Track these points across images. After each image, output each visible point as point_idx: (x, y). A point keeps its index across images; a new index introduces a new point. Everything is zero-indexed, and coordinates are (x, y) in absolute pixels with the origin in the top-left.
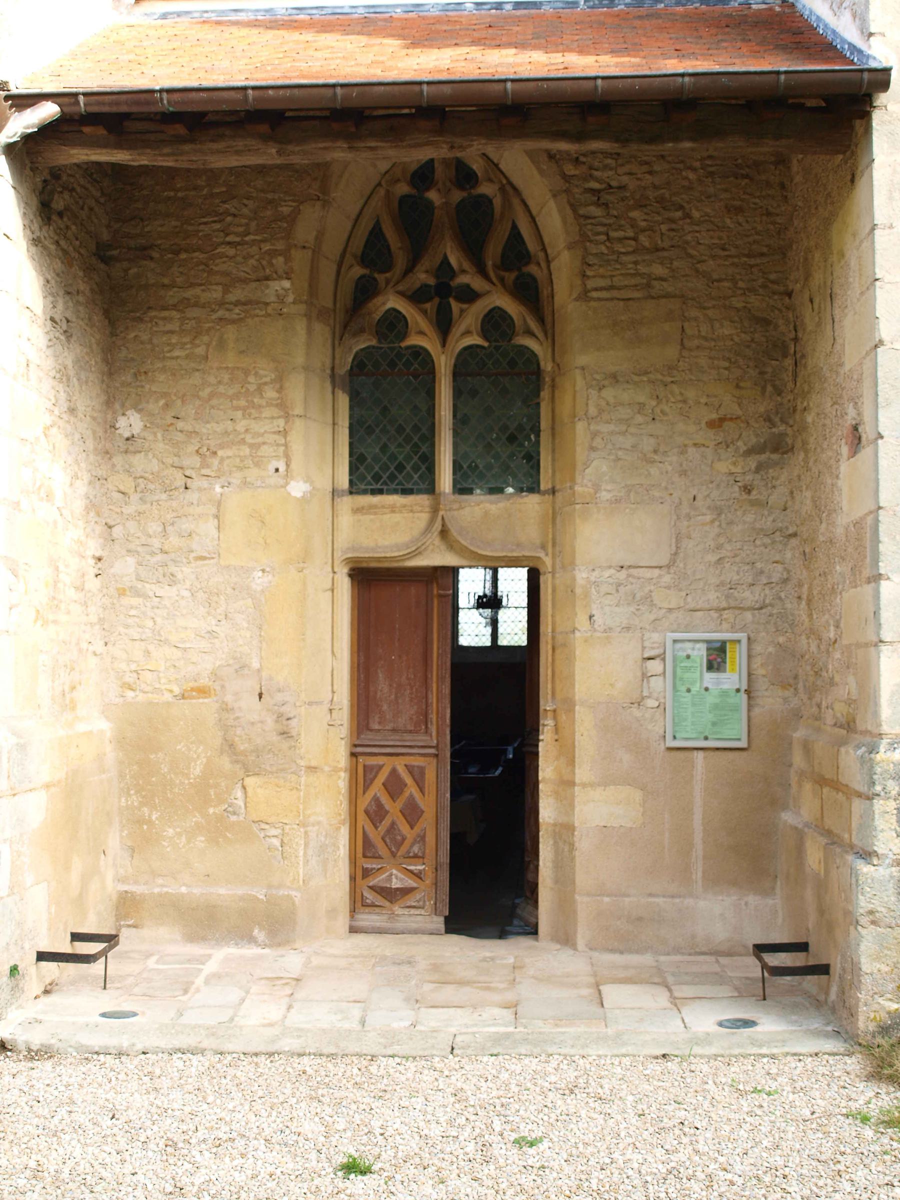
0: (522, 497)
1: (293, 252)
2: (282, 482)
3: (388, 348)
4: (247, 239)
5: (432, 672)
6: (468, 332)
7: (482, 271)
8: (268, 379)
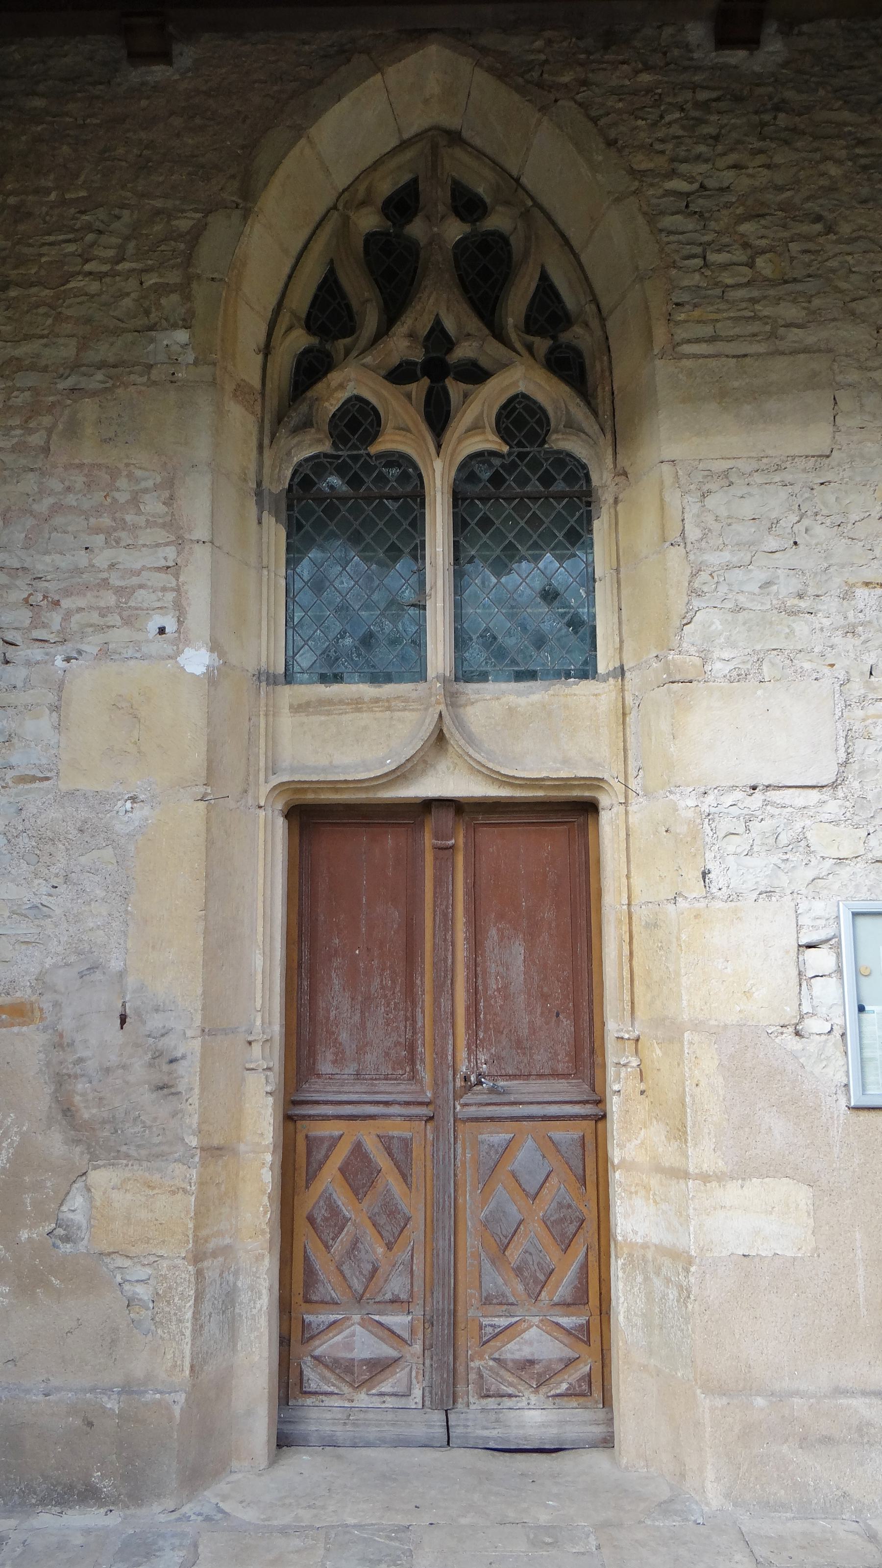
0: (569, 686)
1: (195, 285)
2: (169, 650)
3: (349, 456)
4: (119, 267)
5: (423, 975)
6: (476, 427)
7: (500, 336)
8: (150, 484)
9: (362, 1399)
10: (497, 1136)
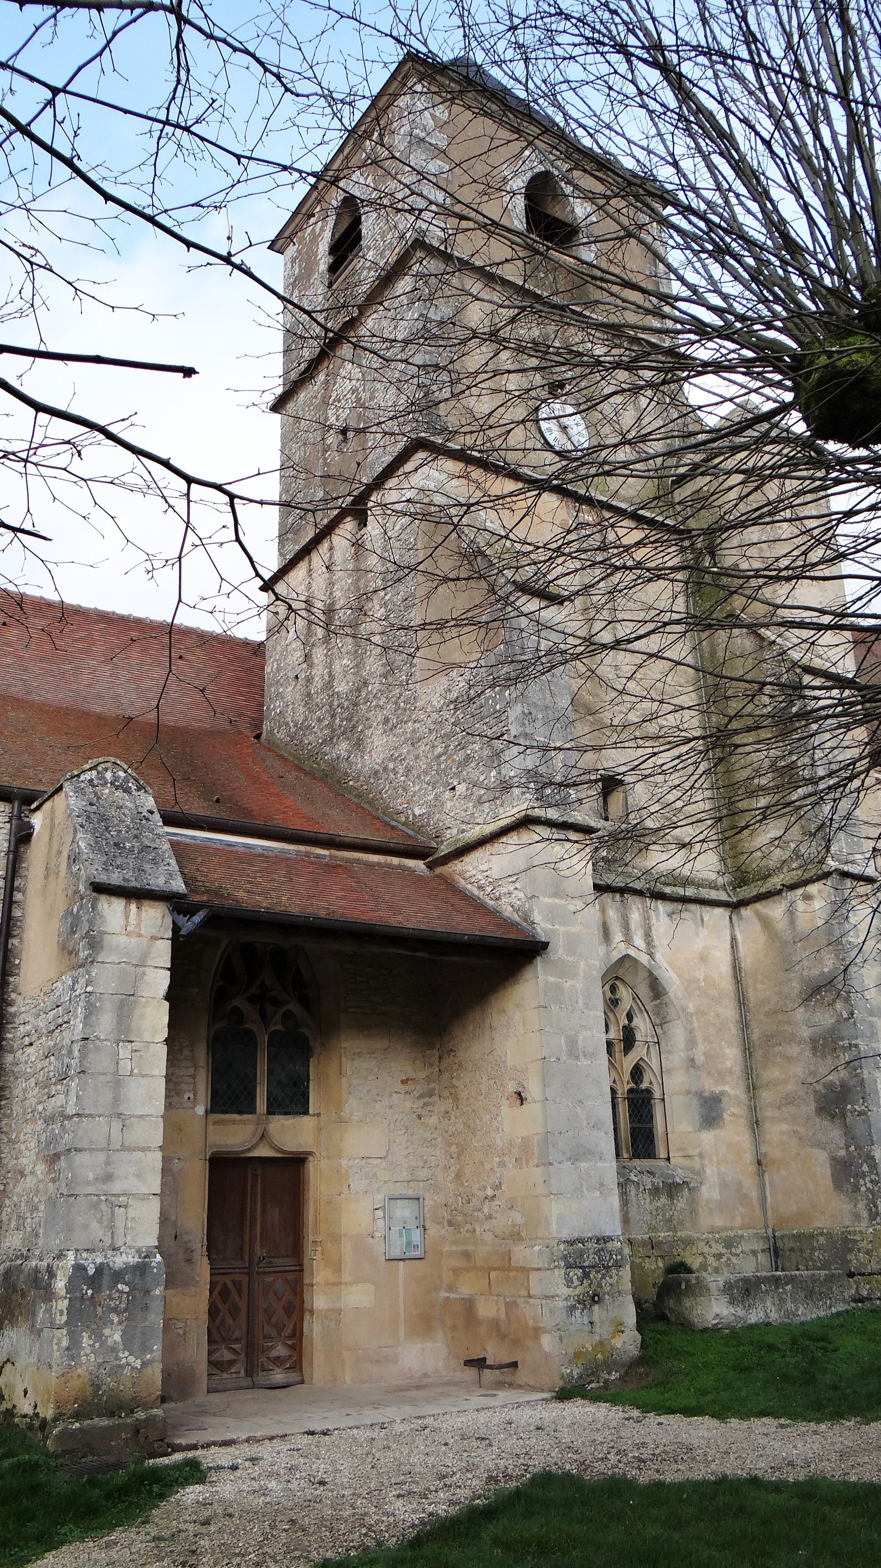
6: (275, 1024)
9: (225, 1375)
10: (269, 1279)
